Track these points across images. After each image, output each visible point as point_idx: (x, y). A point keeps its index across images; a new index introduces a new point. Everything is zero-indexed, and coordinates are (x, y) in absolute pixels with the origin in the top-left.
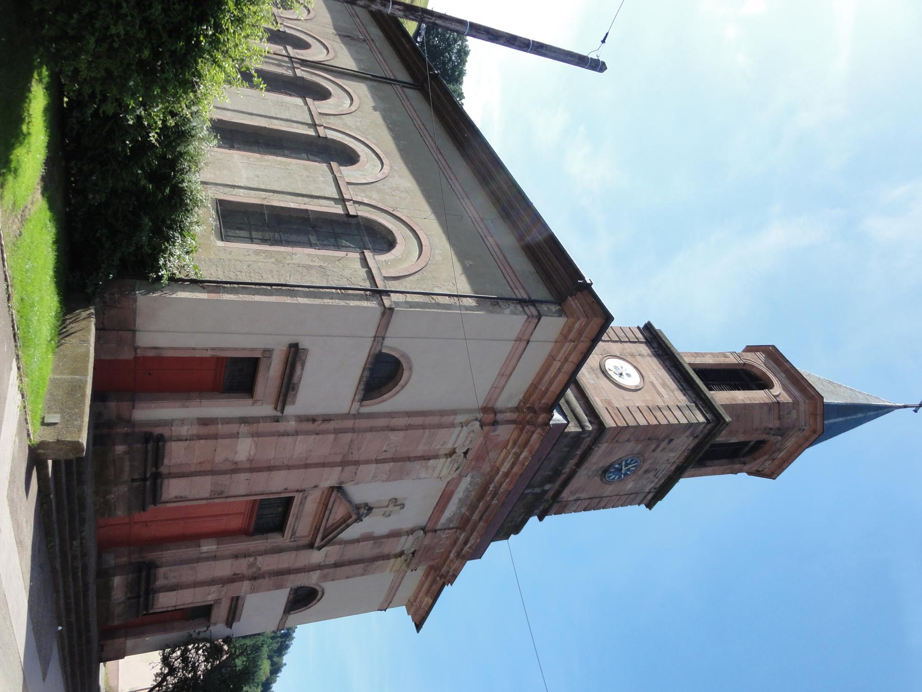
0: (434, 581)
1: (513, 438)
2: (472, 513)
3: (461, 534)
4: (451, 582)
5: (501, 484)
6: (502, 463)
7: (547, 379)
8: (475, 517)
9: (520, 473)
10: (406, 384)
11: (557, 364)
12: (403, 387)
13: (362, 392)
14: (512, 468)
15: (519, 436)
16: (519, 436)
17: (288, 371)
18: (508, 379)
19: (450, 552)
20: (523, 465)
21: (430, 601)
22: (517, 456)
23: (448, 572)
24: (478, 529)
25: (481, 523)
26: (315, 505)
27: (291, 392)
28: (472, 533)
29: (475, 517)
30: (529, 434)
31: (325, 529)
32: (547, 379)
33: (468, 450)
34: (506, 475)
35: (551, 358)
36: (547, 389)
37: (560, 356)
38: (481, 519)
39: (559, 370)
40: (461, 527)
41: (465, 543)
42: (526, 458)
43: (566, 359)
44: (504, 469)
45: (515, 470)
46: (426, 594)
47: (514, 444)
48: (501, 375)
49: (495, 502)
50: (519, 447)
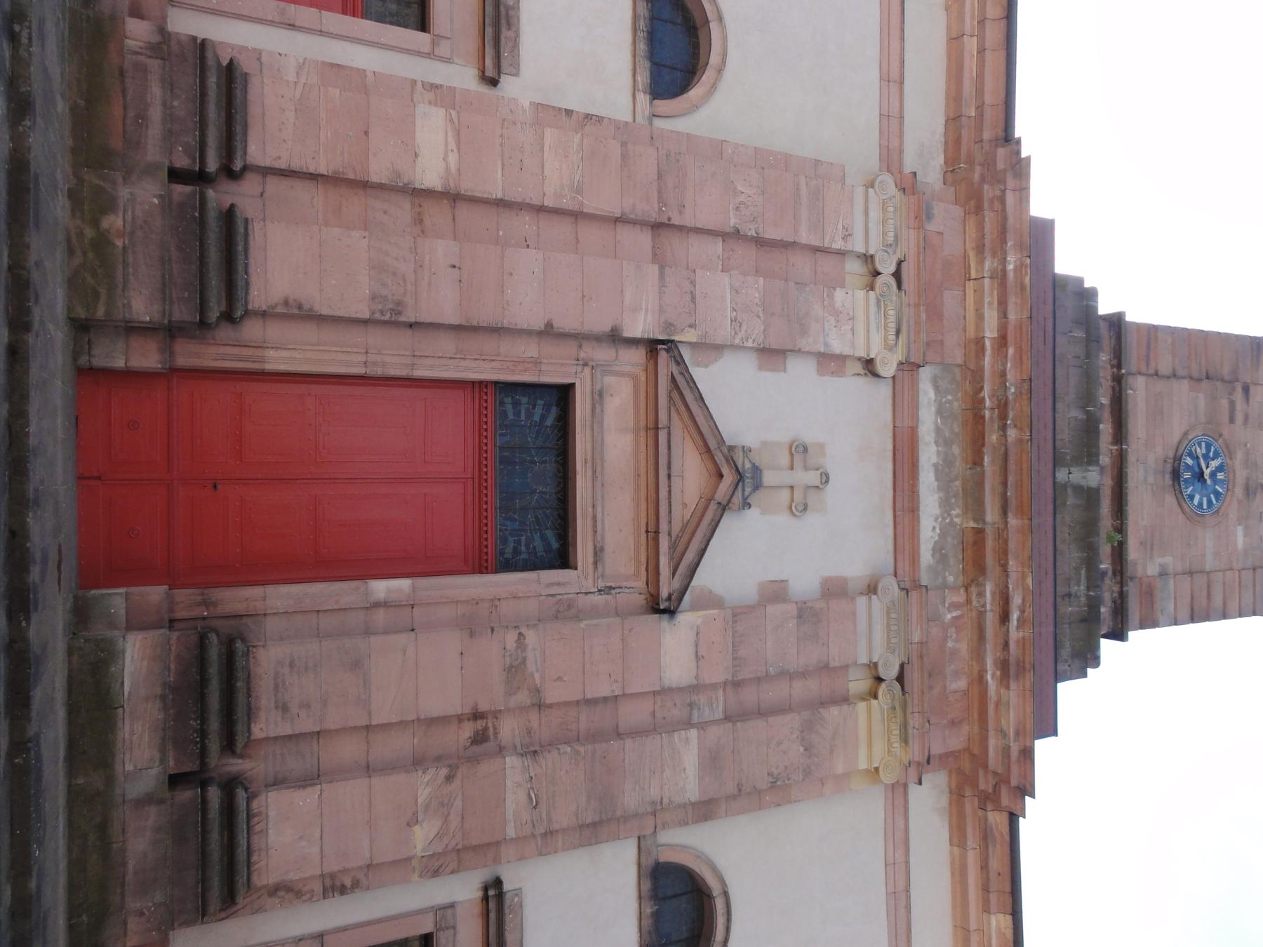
0: (986, 836)
1: (970, 245)
2: (979, 516)
3: (981, 594)
4: (1026, 789)
5: (1003, 374)
6: (980, 317)
7: (968, 87)
8: (991, 514)
9: (1026, 314)
10: (724, 62)
11: (971, 44)
12: (720, 71)
13: (647, 64)
14: (1004, 314)
15: (980, 227)
16: (980, 227)
17: (492, 930)
18: (902, 83)
19: (981, 679)
20: (1023, 288)
21: (1005, 921)
22: (1000, 277)
23: (1006, 750)
24: (1012, 545)
25: (1013, 521)
26: (629, 438)
27: (505, 34)
28: (1004, 568)
29: (991, 514)
30: (997, 205)
31: (673, 547)
32: (968, 87)
33: (899, 264)
34: (1002, 341)
35: (955, 40)
36: (980, 108)
37: (969, 24)
38: (1004, 511)
39: (981, 51)
40: (976, 568)
41: (1005, 617)
42: (1019, 268)
43: (982, 22)
44: (990, 332)
45: (1012, 316)
46: (986, 909)
47: (980, 249)
48: (885, 79)
49: (1012, 434)
50: (994, 255)
